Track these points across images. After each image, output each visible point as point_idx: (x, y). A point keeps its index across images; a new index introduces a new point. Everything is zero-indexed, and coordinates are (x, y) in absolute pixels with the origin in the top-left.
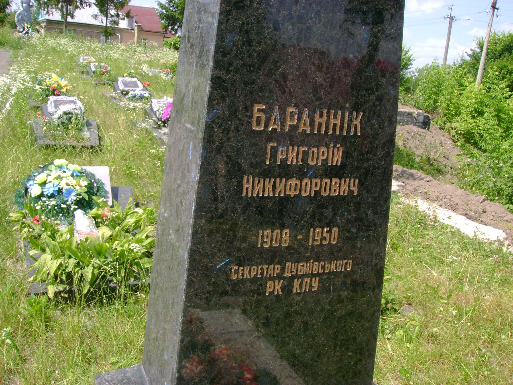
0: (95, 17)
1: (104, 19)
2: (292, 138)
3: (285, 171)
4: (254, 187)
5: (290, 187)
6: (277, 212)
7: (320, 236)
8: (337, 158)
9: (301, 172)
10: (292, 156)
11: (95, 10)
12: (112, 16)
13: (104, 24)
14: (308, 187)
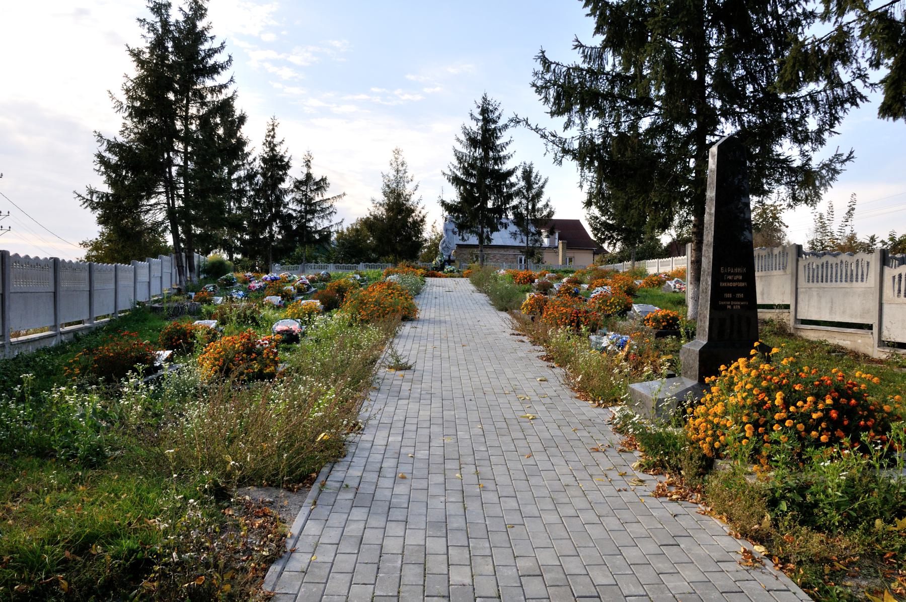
0: (514, 235)
1: (525, 238)
2: (730, 274)
3: (729, 281)
4: (723, 284)
5: (730, 284)
6: (728, 290)
7: (738, 295)
8: (741, 278)
9: (733, 281)
10: (730, 277)
11: (513, 228)
12: (533, 234)
13: (525, 245)
14: (735, 284)
